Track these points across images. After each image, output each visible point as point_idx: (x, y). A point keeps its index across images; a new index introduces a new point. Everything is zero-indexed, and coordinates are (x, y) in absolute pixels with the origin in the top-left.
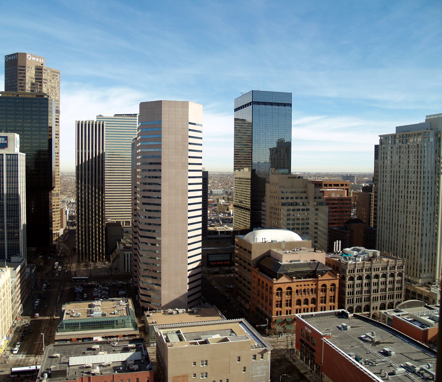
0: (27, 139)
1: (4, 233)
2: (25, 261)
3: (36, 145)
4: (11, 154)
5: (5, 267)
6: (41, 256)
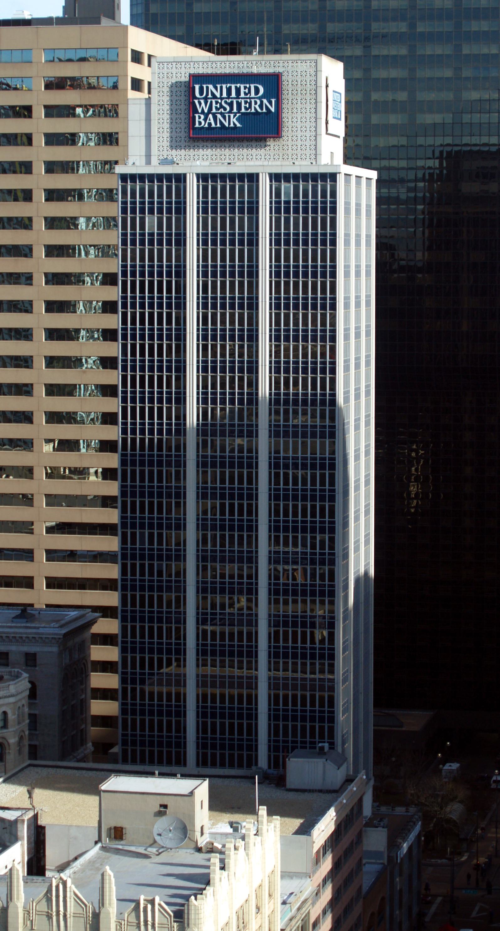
0: (388, 84)
1: (253, 621)
2: (363, 789)
3: (438, 118)
4: (296, 177)
5: (253, 811)
6: (455, 766)
